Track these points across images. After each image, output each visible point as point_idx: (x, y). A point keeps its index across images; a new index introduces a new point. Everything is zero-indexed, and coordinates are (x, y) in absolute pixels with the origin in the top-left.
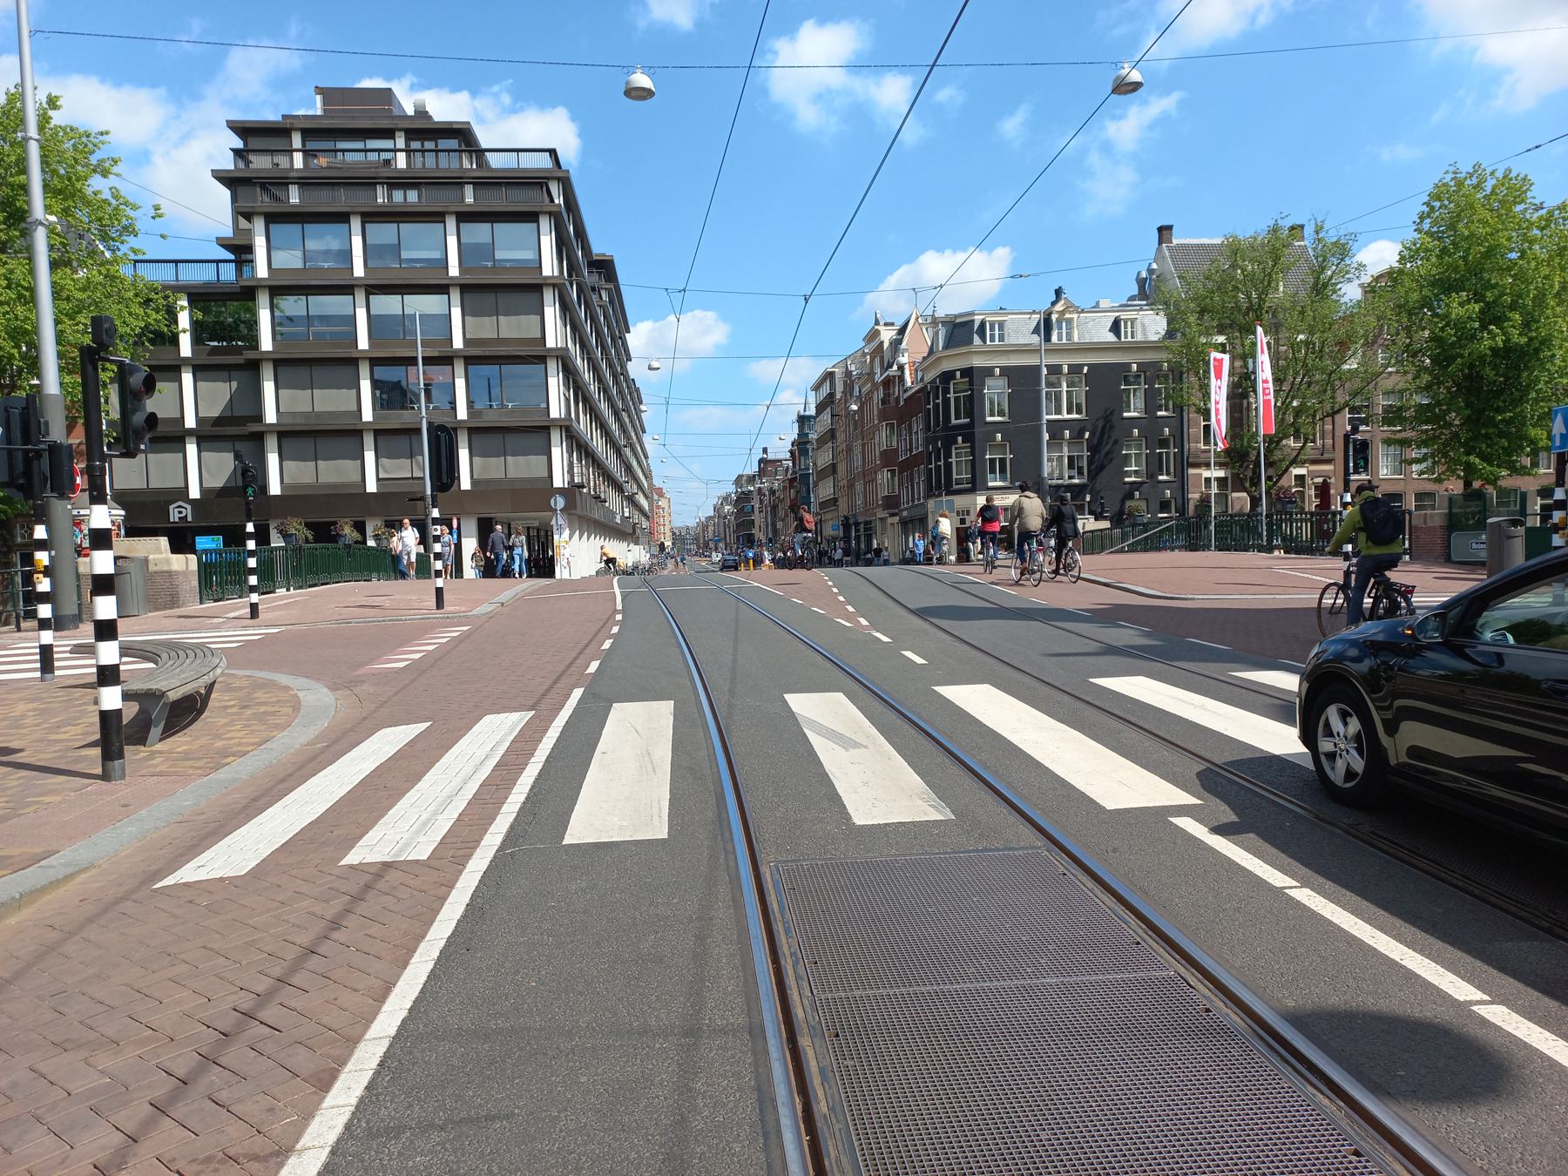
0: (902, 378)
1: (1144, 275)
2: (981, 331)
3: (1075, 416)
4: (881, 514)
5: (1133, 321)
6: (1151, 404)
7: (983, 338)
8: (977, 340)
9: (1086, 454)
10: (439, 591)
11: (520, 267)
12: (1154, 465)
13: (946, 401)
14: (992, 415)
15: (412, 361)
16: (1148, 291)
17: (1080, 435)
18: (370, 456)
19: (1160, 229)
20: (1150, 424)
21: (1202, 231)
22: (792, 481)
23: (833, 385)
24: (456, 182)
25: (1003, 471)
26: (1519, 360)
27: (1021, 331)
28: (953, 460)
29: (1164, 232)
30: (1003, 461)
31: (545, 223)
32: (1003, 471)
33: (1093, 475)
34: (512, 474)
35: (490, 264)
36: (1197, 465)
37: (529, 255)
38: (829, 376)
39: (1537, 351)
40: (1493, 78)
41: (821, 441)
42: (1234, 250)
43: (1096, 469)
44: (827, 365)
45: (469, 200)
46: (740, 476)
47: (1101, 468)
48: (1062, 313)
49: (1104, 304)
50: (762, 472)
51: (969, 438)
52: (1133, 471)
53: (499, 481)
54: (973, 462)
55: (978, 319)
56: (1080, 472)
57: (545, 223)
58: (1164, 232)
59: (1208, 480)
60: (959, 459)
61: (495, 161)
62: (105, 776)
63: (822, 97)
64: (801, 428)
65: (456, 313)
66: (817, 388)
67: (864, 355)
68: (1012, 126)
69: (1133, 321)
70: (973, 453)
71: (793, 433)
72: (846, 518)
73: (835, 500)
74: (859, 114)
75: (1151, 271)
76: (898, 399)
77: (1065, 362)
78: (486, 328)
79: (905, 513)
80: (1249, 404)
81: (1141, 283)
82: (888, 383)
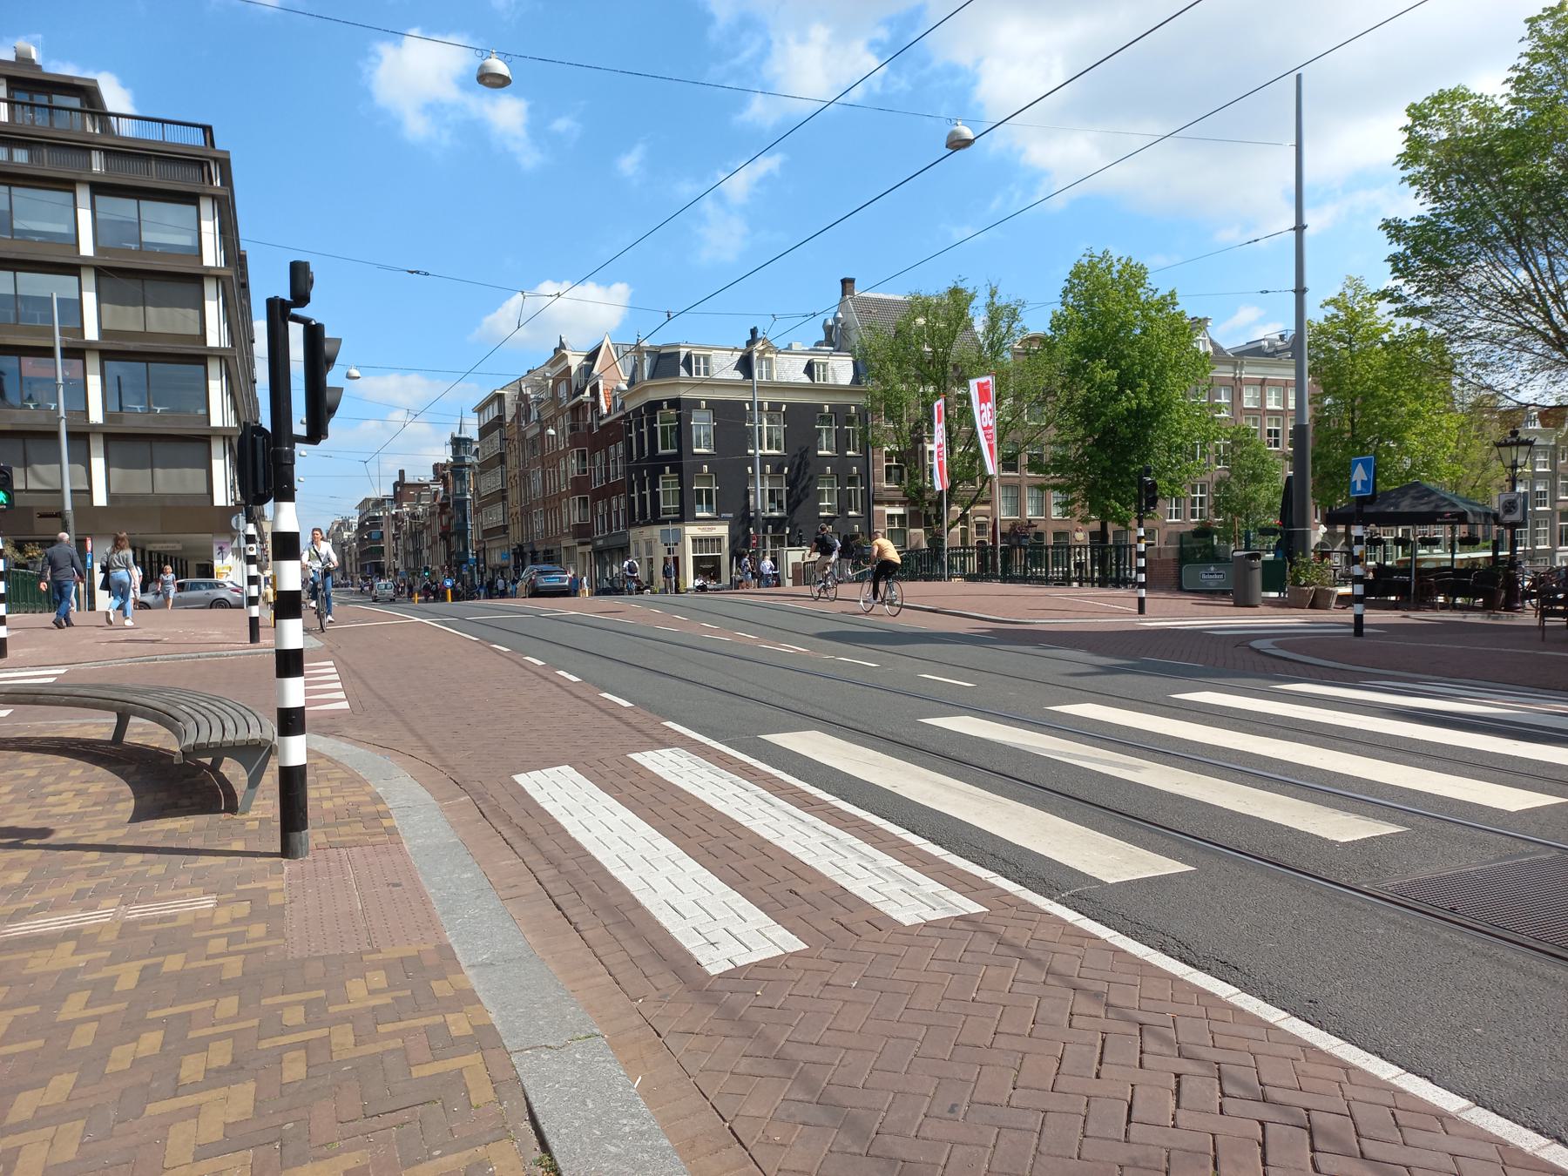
0: (596, 405)
1: (830, 322)
2: (688, 362)
3: (670, 451)
4: (568, 542)
5: (825, 365)
6: (842, 442)
7: (690, 371)
8: (683, 372)
9: (785, 488)
10: (254, 622)
11: (170, 252)
12: (844, 503)
13: (653, 432)
14: (699, 446)
15: (48, 352)
16: (835, 338)
17: (779, 470)
18: (98, 464)
19: (844, 282)
20: (841, 462)
21: (888, 287)
22: (444, 506)
23: (502, 407)
24: (84, 148)
25: (709, 502)
26: (1143, 419)
27: (724, 366)
28: (660, 489)
29: (847, 283)
30: (709, 492)
31: (206, 207)
32: (709, 502)
33: (792, 508)
34: (161, 488)
35: (133, 247)
36: (881, 503)
37: (187, 240)
38: (499, 398)
39: (1159, 414)
40: (1035, 177)
41: (486, 466)
42: (922, 306)
43: (794, 504)
44: (496, 386)
45: (96, 168)
46: (367, 500)
47: (798, 502)
48: (762, 352)
49: (796, 347)
50: (397, 498)
51: (678, 469)
52: (827, 505)
53: (143, 496)
54: (681, 492)
55: (683, 352)
56: (780, 506)
57: (206, 207)
58: (847, 283)
59: (891, 517)
60: (667, 487)
61: (126, 129)
62: (287, 851)
63: (433, 109)
64: (455, 451)
65: (90, 300)
66: (480, 409)
67: (546, 379)
68: (629, 164)
69: (825, 365)
70: (681, 484)
71: (445, 455)
72: (520, 547)
73: (505, 528)
74: (475, 133)
75: (836, 320)
76: (590, 427)
77: (767, 399)
78: (129, 319)
79: (600, 543)
80: (924, 448)
81: (828, 330)
82: (578, 409)
